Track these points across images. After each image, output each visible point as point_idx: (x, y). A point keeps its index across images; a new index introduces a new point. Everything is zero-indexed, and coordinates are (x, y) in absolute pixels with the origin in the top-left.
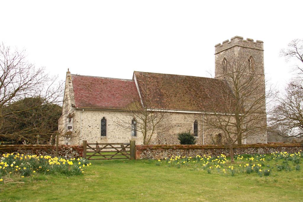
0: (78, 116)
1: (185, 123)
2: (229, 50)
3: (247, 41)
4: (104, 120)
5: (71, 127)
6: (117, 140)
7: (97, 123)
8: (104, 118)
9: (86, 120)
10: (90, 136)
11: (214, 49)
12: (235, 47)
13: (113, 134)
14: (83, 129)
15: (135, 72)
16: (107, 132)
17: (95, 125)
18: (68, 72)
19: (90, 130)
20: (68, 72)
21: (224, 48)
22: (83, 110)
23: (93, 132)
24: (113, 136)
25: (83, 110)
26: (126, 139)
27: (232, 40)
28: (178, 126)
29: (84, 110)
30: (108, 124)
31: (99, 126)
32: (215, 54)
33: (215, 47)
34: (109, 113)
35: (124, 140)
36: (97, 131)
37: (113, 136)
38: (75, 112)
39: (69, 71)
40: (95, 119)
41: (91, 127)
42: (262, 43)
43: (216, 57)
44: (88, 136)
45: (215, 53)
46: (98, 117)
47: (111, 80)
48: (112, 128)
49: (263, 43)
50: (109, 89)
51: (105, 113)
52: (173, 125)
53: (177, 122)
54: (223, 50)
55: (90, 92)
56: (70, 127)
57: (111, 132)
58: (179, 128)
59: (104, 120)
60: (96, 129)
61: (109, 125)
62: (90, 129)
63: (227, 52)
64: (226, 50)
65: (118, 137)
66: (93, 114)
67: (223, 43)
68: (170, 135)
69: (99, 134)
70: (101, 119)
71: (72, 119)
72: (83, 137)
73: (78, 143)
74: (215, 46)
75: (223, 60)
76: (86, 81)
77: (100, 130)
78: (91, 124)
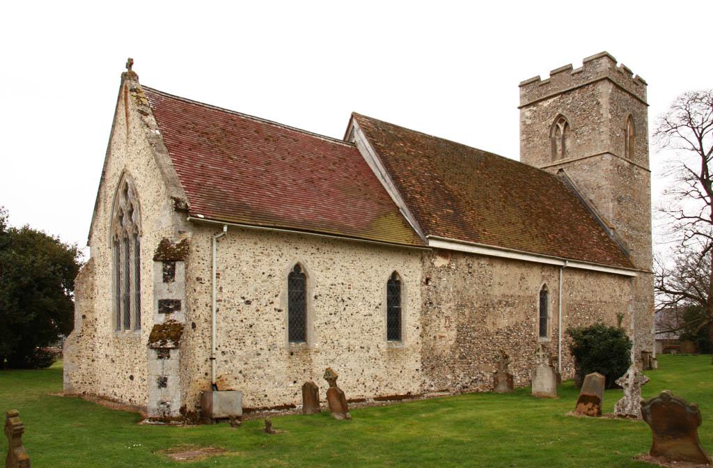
0: (201, 254)
1: (522, 294)
2: (576, 94)
3: (623, 71)
4: (297, 279)
5: (177, 305)
6: (342, 356)
7: (274, 287)
8: (395, 274)
9: (233, 273)
10: (248, 342)
11: (517, 92)
12: (599, 83)
13: (329, 332)
14: (223, 312)
15: (354, 116)
16: (308, 327)
17: (267, 297)
18: (129, 76)
19: (247, 315)
20: (129, 76)
21: (556, 87)
22: (225, 229)
23: (263, 327)
24: (329, 341)
25: (225, 229)
26: (372, 352)
27: (587, 63)
28: (507, 304)
29: (228, 226)
30: (312, 291)
31: (282, 302)
32: (520, 108)
33: (520, 86)
34: (314, 251)
35: (367, 354)
36: (276, 323)
37: (329, 341)
38: (189, 235)
39: (134, 69)
40: (266, 269)
41: (254, 304)
42: (644, 86)
43: (522, 115)
44: (241, 341)
45: (519, 105)
46: (377, 269)
47: (286, 132)
48: (326, 308)
49: (647, 85)
50: (289, 159)
51: (303, 247)
52: (496, 300)
53: (504, 290)
54: (551, 94)
55: (230, 162)
56: (172, 301)
57: (323, 327)
58: (508, 309)
59: (297, 279)
60: (270, 312)
61: (316, 297)
62: (248, 312)
63: (569, 99)
64: (564, 93)
65: (345, 345)
66: (258, 248)
67: (551, 75)
68: (487, 334)
69: (282, 337)
70: (288, 272)
71: (180, 267)
72: (223, 349)
73: (203, 375)
74: (519, 84)
75: (554, 123)
76: (200, 121)
77: (284, 315)
78: (251, 289)
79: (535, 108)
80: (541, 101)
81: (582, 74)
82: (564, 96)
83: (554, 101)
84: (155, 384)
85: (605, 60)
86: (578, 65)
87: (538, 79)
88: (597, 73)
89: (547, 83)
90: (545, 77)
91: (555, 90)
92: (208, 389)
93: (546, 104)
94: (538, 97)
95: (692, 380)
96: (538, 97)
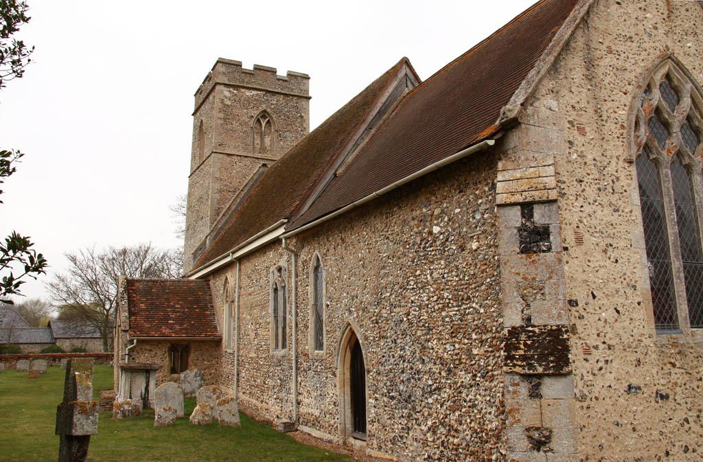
67: (255, 68)
79: (235, 92)
80: (243, 87)
81: (286, 83)
82: (268, 94)
83: (257, 95)
84: (632, 431)
85: (220, 64)
86: (282, 73)
87: (238, 65)
88: (301, 90)
89: (247, 73)
90: (282, 73)
91: (259, 84)
92: (44, 321)
93: (248, 93)
94: (240, 83)
95: (699, 459)
96: (240, 83)
